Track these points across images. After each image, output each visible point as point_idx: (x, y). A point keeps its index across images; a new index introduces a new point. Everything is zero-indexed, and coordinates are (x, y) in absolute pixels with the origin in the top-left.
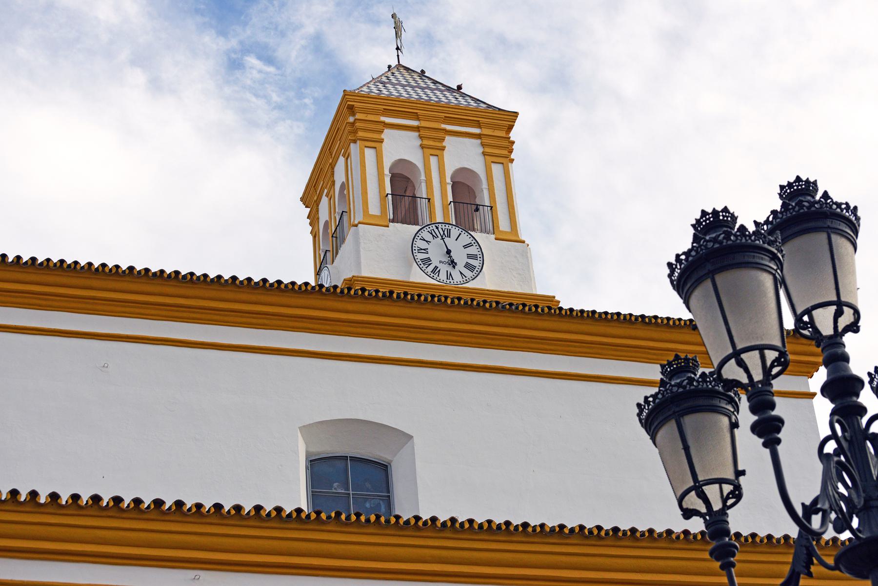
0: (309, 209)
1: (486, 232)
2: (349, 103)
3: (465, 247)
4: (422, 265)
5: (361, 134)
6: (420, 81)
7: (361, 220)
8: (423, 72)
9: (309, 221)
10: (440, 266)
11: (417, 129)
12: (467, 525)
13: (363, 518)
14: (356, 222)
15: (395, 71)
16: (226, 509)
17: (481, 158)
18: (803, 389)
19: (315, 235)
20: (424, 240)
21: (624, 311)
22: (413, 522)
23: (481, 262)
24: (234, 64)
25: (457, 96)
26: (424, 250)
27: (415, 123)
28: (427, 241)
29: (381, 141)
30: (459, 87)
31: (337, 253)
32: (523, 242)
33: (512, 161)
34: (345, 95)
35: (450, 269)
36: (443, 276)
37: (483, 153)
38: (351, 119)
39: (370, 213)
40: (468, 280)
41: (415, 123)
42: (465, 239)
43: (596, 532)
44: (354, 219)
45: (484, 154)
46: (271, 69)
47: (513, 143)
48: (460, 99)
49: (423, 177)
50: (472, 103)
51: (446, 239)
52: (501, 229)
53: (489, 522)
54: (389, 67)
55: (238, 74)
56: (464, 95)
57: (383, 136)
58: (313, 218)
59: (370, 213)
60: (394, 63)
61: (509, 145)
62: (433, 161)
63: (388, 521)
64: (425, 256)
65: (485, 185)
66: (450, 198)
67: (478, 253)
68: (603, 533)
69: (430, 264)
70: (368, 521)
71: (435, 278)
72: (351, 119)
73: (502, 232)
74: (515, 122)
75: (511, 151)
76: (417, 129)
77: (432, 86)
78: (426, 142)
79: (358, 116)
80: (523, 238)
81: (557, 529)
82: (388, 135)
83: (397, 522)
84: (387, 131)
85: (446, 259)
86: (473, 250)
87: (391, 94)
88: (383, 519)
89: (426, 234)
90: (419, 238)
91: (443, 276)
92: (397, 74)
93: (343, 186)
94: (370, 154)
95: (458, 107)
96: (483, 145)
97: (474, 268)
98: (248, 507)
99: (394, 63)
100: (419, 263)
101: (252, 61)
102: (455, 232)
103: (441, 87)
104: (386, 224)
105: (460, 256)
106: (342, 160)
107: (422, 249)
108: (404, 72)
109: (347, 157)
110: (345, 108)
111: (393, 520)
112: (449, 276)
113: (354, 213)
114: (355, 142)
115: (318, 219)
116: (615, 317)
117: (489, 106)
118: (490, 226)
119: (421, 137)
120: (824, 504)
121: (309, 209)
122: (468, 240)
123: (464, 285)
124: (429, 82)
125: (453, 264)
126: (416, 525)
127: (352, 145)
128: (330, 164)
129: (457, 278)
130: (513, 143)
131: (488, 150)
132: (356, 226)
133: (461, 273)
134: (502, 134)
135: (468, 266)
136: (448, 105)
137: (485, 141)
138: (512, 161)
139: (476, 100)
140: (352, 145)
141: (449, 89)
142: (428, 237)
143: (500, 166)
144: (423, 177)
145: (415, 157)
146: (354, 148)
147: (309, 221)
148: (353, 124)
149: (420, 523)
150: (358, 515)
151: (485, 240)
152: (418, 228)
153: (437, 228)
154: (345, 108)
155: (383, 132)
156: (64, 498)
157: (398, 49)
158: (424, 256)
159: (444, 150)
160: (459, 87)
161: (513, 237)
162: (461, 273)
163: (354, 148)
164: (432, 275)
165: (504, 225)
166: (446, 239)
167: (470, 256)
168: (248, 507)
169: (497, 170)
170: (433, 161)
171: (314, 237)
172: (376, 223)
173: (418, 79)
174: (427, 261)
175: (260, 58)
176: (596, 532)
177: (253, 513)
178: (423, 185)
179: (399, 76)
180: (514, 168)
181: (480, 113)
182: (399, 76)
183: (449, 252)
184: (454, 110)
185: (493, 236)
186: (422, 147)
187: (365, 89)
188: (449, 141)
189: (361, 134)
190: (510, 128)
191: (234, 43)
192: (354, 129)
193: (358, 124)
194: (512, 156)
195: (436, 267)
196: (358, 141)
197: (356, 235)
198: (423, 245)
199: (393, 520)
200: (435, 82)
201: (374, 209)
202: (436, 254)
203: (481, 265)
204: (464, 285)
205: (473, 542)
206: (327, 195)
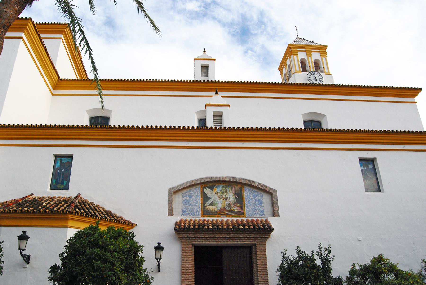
0: (280, 71)
3: (319, 76)
5: (293, 53)
6: (304, 41)
7: (295, 72)
8: (304, 39)
9: (280, 74)
10: (314, 81)
11: (305, 51)
12: (359, 131)
13: (319, 130)
14: (294, 73)
15: (297, 39)
16: (231, 128)
17: (306, 56)
18: (414, 101)
19: (282, 77)
21: (371, 85)
22: (347, 130)
24: (246, 52)
25: (313, 43)
27: (304, 50)
30: (313, 41)
31: (289, 81)
32: (331, 74)
33: (327, 57)
34: (289, 45)
35: (316, 81)
38: (290, 50)
39: (297, 70)
41: (304, 50)
42: (318, 75)
43: (388, 131)
44: (293, 72)
45: (321, 55)
46: (253, 53)
47: (327, 52)
48: (314, 44)
49: (308, 62)
50: (316, 44)
51: (314, 75)
52: (326, 72)
53: (364, 130)
54: (296, 38)
55: (246, 54)
56: (314, 43)
57: (298, 53)
58: (281, 73)
59: (297, 70)
60: (297, 37)
61: (326, 53)
63: (320, 130)
64: (310, 79)
65: (321, 63)
68: (390, 132)
70: (316, 130)
72: (290, 50)
73: (326, 72)
76: (305, 51)
77: (306, 41)
78: (307, 54)
79: (292, 49)
80: (331, 74)
81: (380, 131)
83: (110, 127)
84: (299, 52)
85: (315, 79)
86: (320, 77)
87: (296, 44)
88: (319, 130)
89: (310, 74)
92: (298, 39)
93: (289, 65)
94: (295, 57)
95: (314, 45)
96: (320, 53)
98: (245, 128)
99: (297, 37)
101: (249, 51)
102: (316, 73)
103: (308, 42)
104: (301, 72)
105: (318, 78)
106: (288, 59)
108: (300, 39)
109: (290, 58)
111: (322, 130)
113: (293, 71)
114: (292, 55)
115: (283, 73)
116: (369, 87)
117: (320, 45)
118: (323, 71)
119: (306, 53)
121: (280, 71)
124: (306, 41)
125: (316, 80)
126: (327, 131)
127: (291, 56)
128: (285, 61)
130: (327, 52)
131: (321, 55)
132: (294, 73)
135: (319, 80)
136: (311, 45)
137: (321, 53)
139: (317, 44)
140: (291, 56)
141: (310, 42)
142: (310, 75)
144: (308, 62)
147: (280, 74)
148: (291, 51)
149: (349, 131)
150: (314, 129)
151: (323, 74)
152: (307, 73)
153: (312, 72)
156: (168, 127)
157: (297, 34)
160: (313, 41)
161: (329, 74)
163: (292, 57)
166: (314, 75)
167: (320, 78)
168: (245, 128)
169: (324, 59)
170: (309, 58)
171: (282, 77)
173: (303, 40)
175: (251, 51)
176: (388, 131)
177: (246, 129)
178: (308, 63)
179: (299, 40)
180: (327, 58)
182: (299, 40)
183: (315, 78)
185: (324, 74)
186: (307, 55)
187: (292, 43)
188: (312, 53)
189: (293, 53)
190: (326, 49)
191: (245, 48)
192: (291, 52)
193: (292, 51)
194: (327, 56)
195: (313, 81)
196: (293, 55)
197: (294, 76)
198: (309, 76)
199: (322, 130)
200: (307, 41)
201: (298, 69)
202: (312, 78)
206: (285, 68)
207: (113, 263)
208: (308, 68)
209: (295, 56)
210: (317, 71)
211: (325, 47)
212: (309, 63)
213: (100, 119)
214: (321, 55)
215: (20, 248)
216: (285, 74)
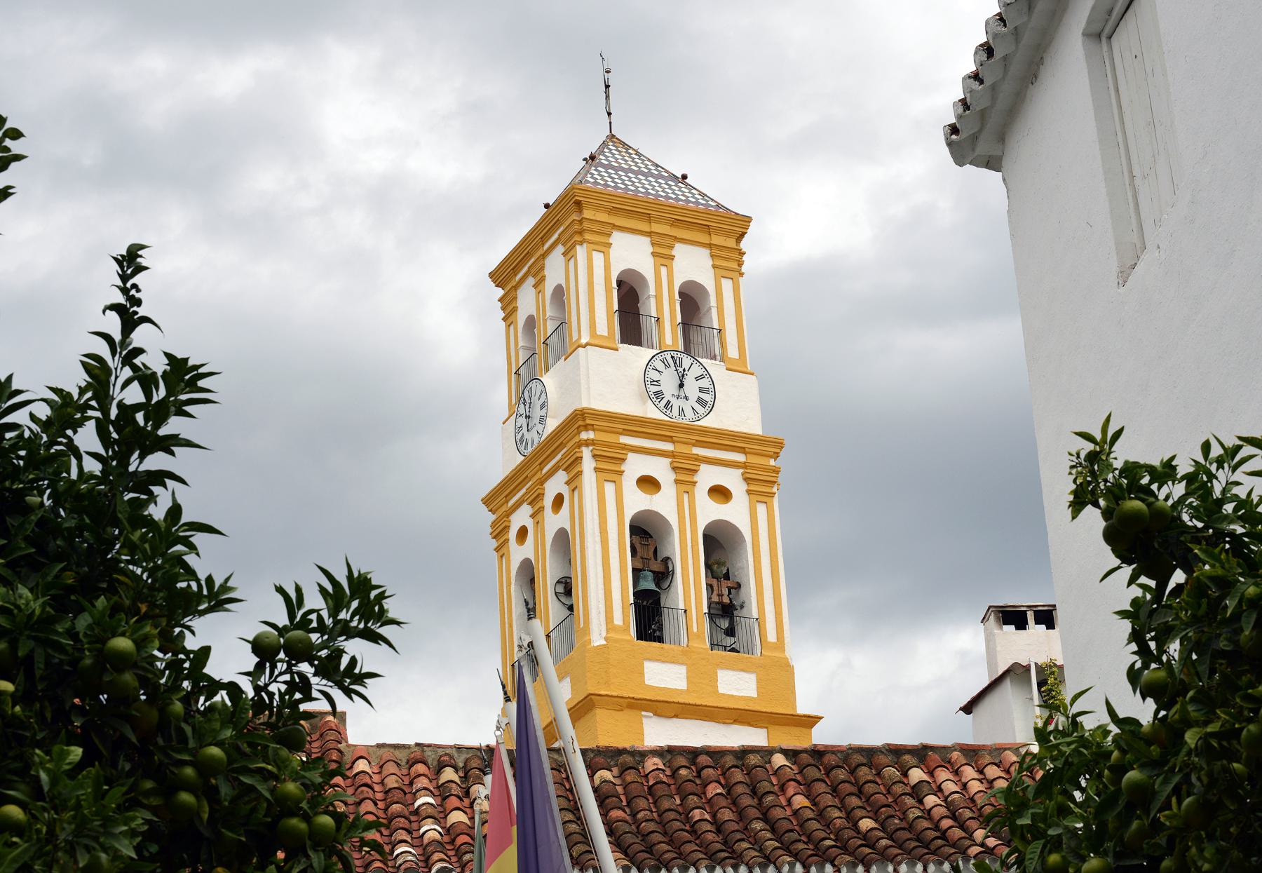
1: (714, 358)
2: (576, 198)
3: (697, 379)
4: (655, 399)
9: (500, 304)
11: (649, 234)
17: (651, 260)
20: (657, 370)
23: (713, 397)
26: (656, 381)
28: (657, 370)
29: (672, 258)
30: (684, 177)
36: (675, 411)
37: (652, 253)
40: (700, 418)
56: (687, 185)
62: (664, 270)
66: (679, 319)
67: (710, 387)
69: (663, 398)
71: (667, 414)
74: (748, 229)
75: (740, 264)
82: (617, 238)
86: (705, 383)
90: (651, 368)
91: (675, 411)
94: (598, 258)
97: (706, 403)
100: (651, 397)
107: (654, 381)
110: (572, 202)
112: (681, 412)
114: (581, 243)
120: (346, 682)
122: (700, 371)
123: (696, 423)
127: (578, 247)
129: (689, 414)
133: (693, 409)
134: (731, 243)
135: (700, 401)
137: (656, 239)
138: (742, 274)
139: (703, 195)
140: (578, 247)
142: (660, 366)
143: (730, 281)
145: (706, 278)
146: (581, 251)
151: (715, 368)
154: (572, 202)
155: (673, 247)
158: (656, 389)
159: (673, 259)
160: (684, 177)
162: (693, 409)
164: (665, 410)
165: (733, 352)
167: (702, 390)
169: (727, 285)
170: (664, 270)
172: (604, 344)
174: (659, 395)
178: (653, 301)
181: (623, 200)
184: (623, 200)
189: (587, 236)
195: (669, 402)
196: (585, 245)
198: (655, 376)
201: (602, 329)
203: (713, 400)
204: (696, 423)
205: (529, 738)
207: (1244, 721)
208: (647, 325)
209: (594, 253)
210: (687, 350)
211: (738, 226)
212: (659, 298)
213: (110, 636)
214: (753, 488)
215: (900, 842)
216: (531, 322)
